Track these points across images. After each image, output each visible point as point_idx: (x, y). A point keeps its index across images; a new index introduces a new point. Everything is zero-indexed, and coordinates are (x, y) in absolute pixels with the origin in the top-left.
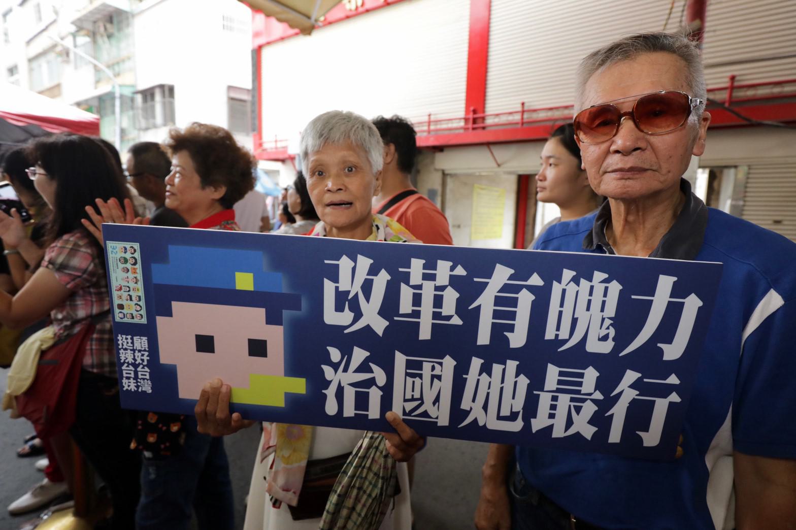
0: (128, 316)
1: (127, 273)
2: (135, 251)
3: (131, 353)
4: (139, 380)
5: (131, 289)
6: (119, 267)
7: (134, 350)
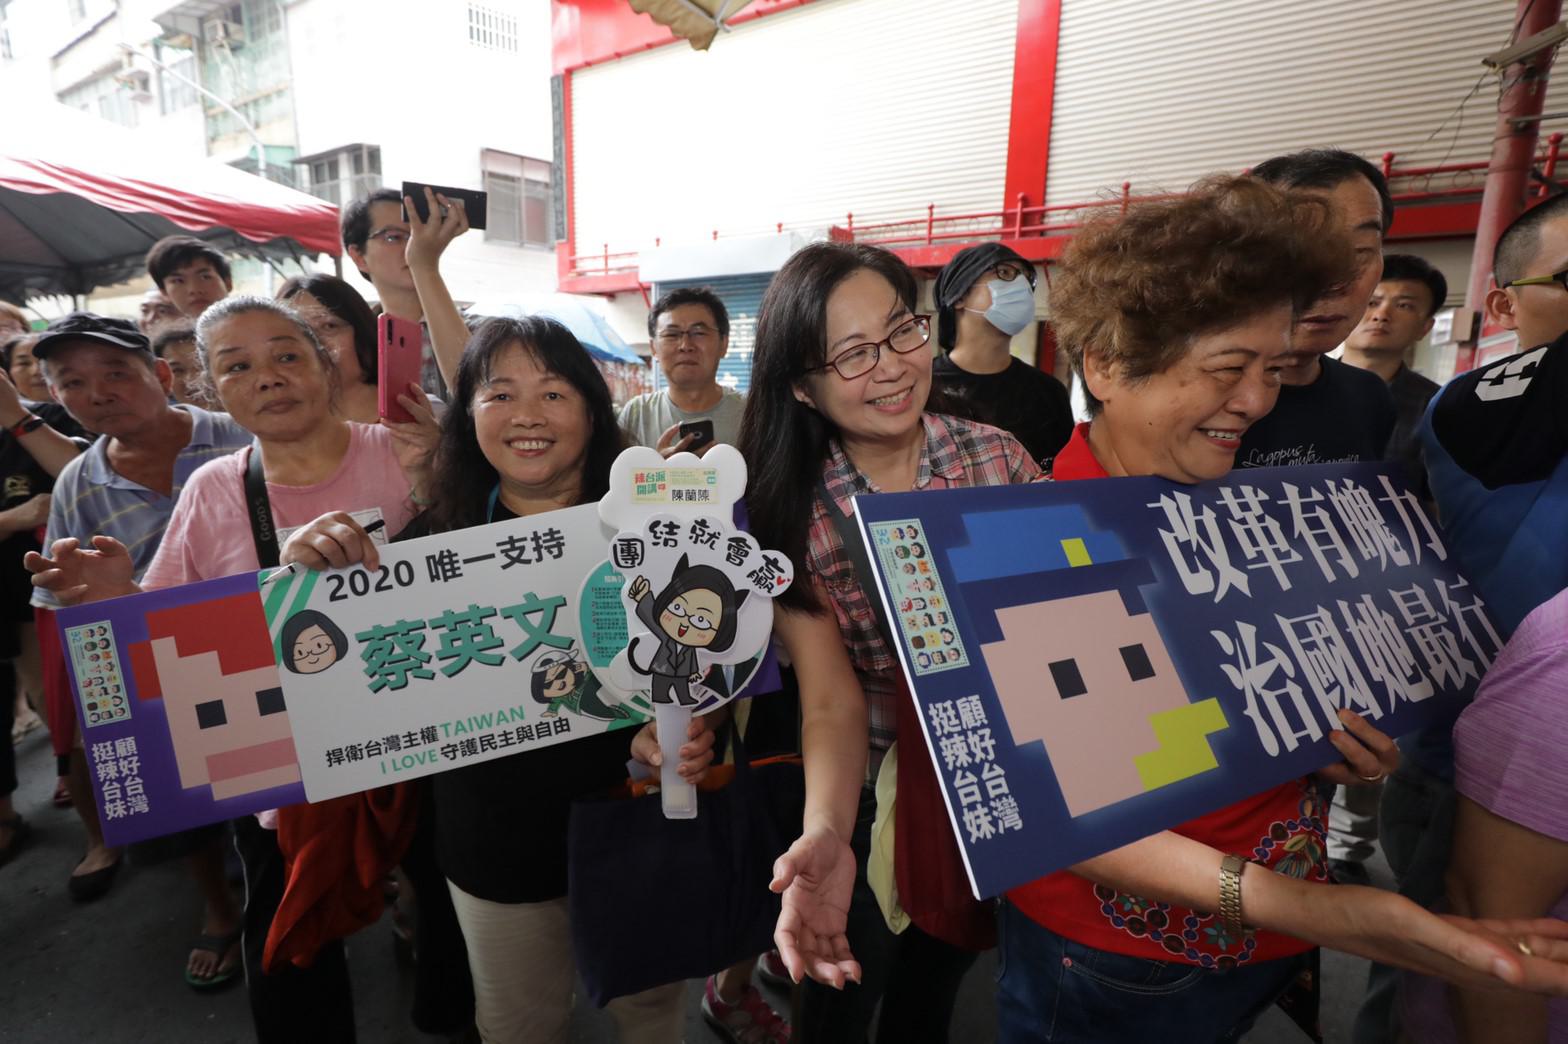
0: (105, 716)
1: (913, 573)
2: (916, 532)
3: (962, 741)
4: (129, 799)
5: (105, 680)
6: (898, 566)
7: (117, 760)
